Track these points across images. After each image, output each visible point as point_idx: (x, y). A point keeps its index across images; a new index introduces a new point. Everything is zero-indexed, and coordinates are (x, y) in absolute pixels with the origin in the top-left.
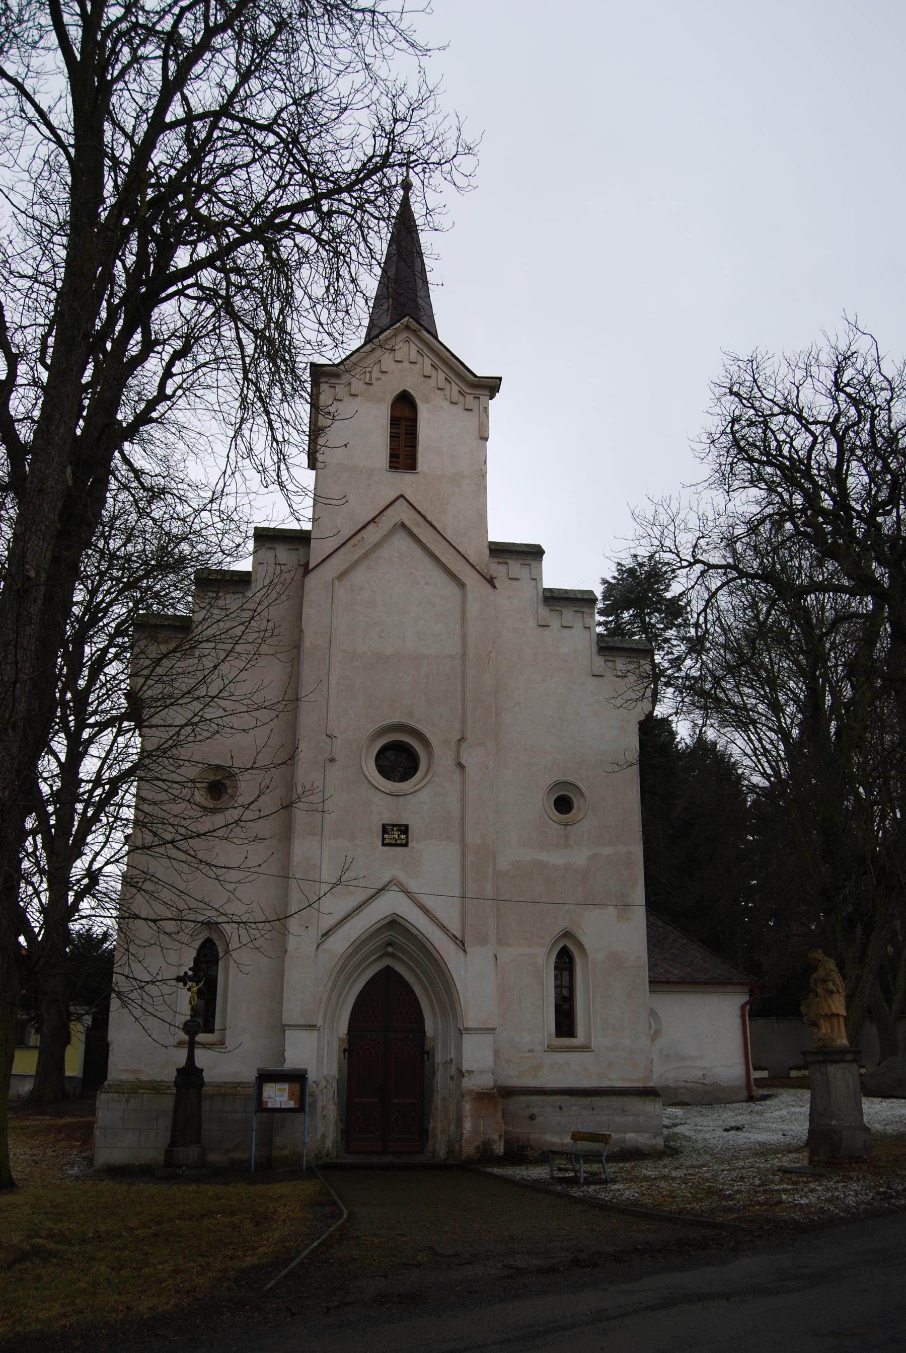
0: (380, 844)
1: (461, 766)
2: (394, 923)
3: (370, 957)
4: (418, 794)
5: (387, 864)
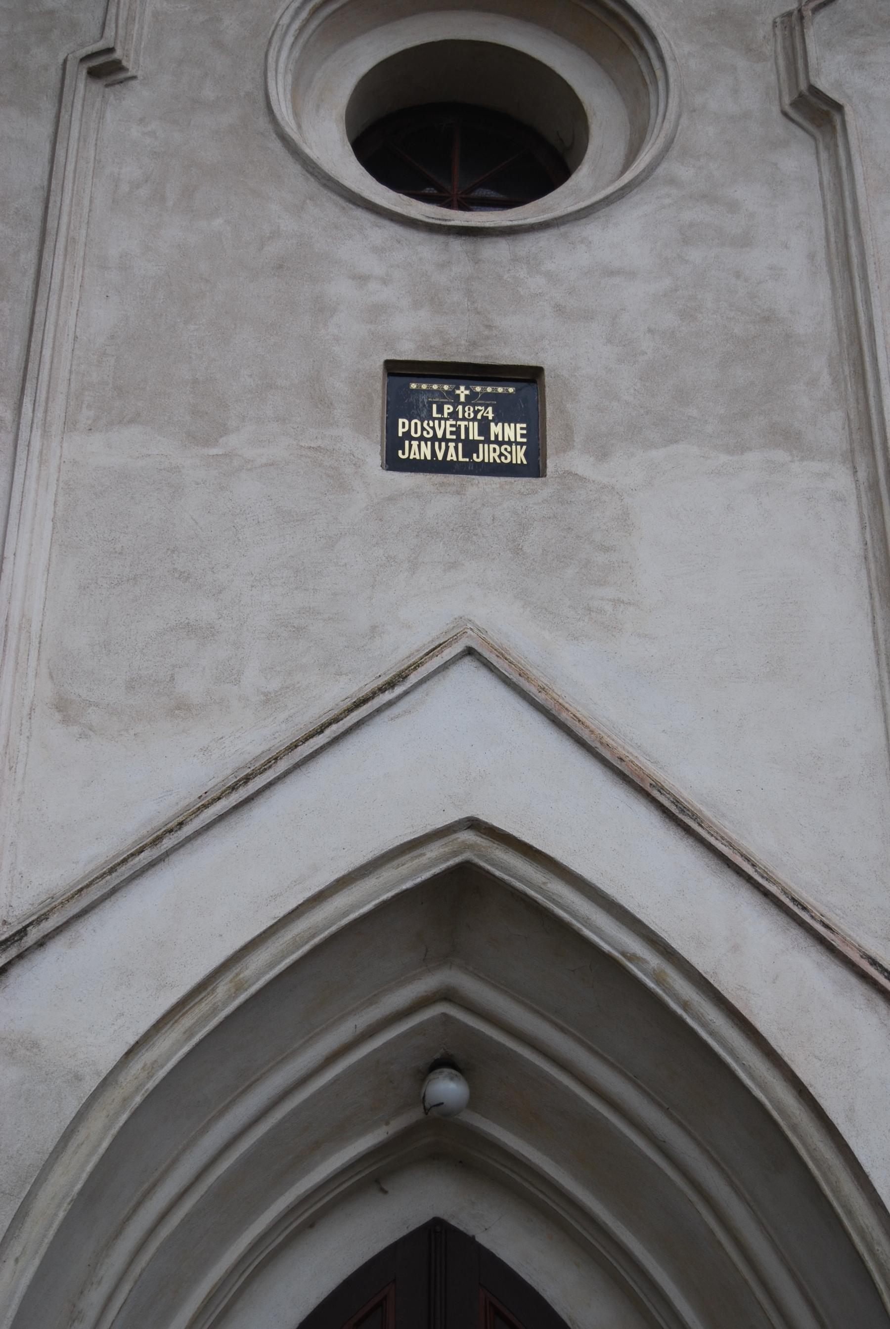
0: (374, 456)
1: (817, 112)
2: (467, 900)
3: (318, 1148)
4: (590, 230)
5: (426, 563)
